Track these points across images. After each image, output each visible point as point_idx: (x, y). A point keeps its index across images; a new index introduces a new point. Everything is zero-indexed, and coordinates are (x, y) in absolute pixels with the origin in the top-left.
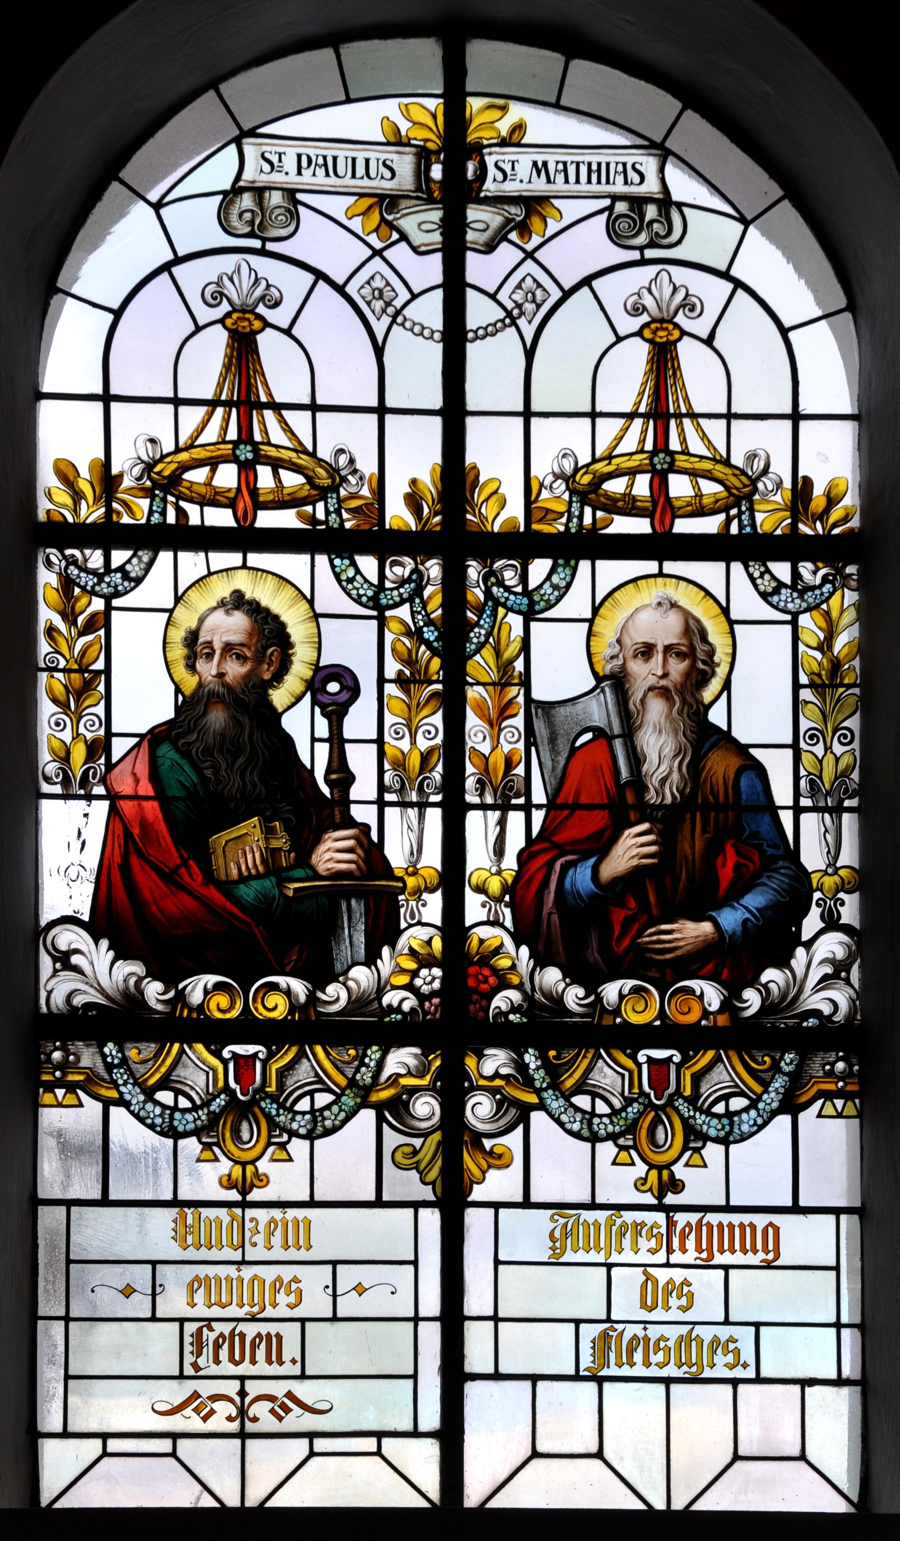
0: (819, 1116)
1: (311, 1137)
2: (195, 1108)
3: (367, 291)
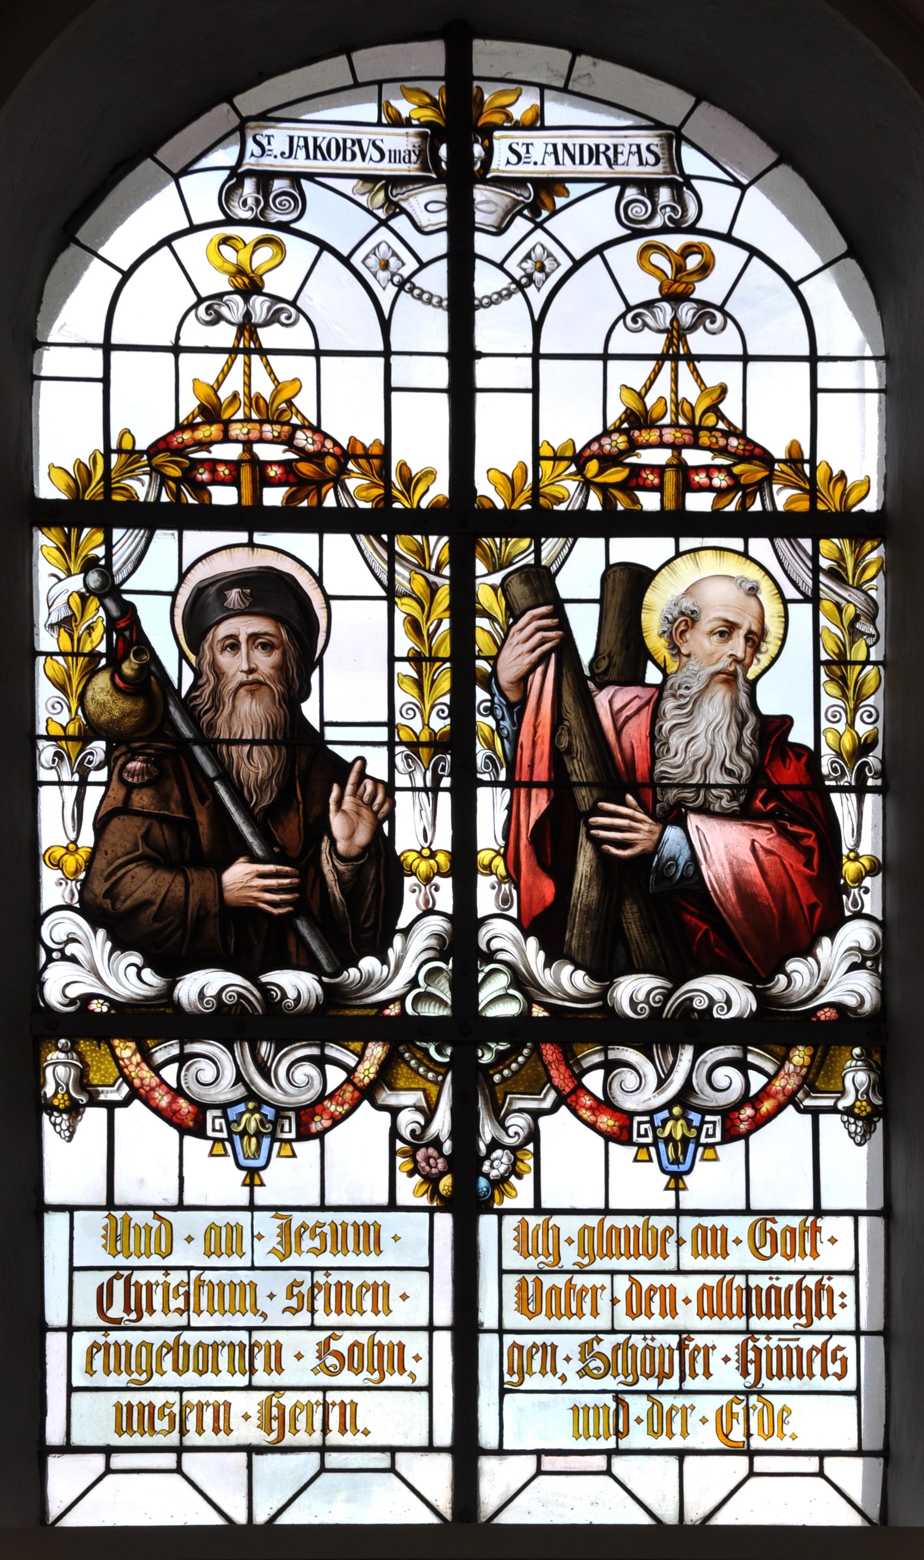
3: (372, 261)
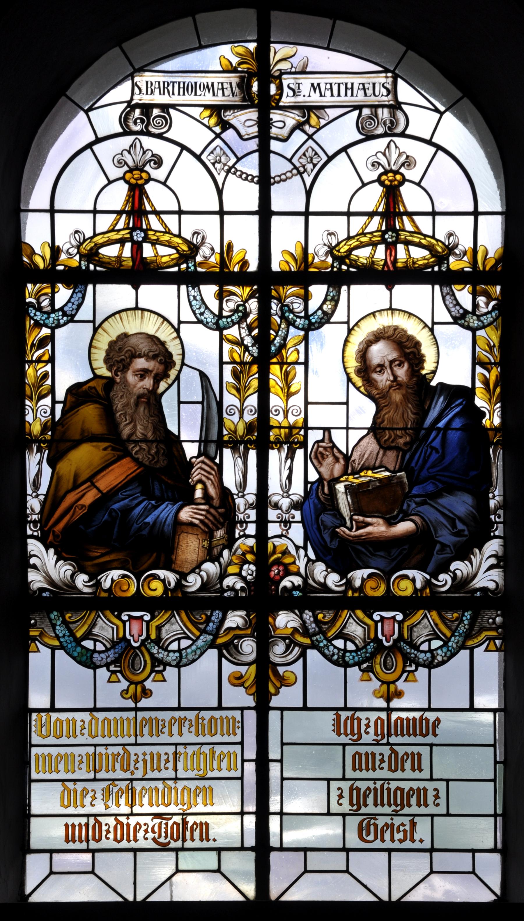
0: (486, 650)
1: (179, 666)
2: (107, 650)
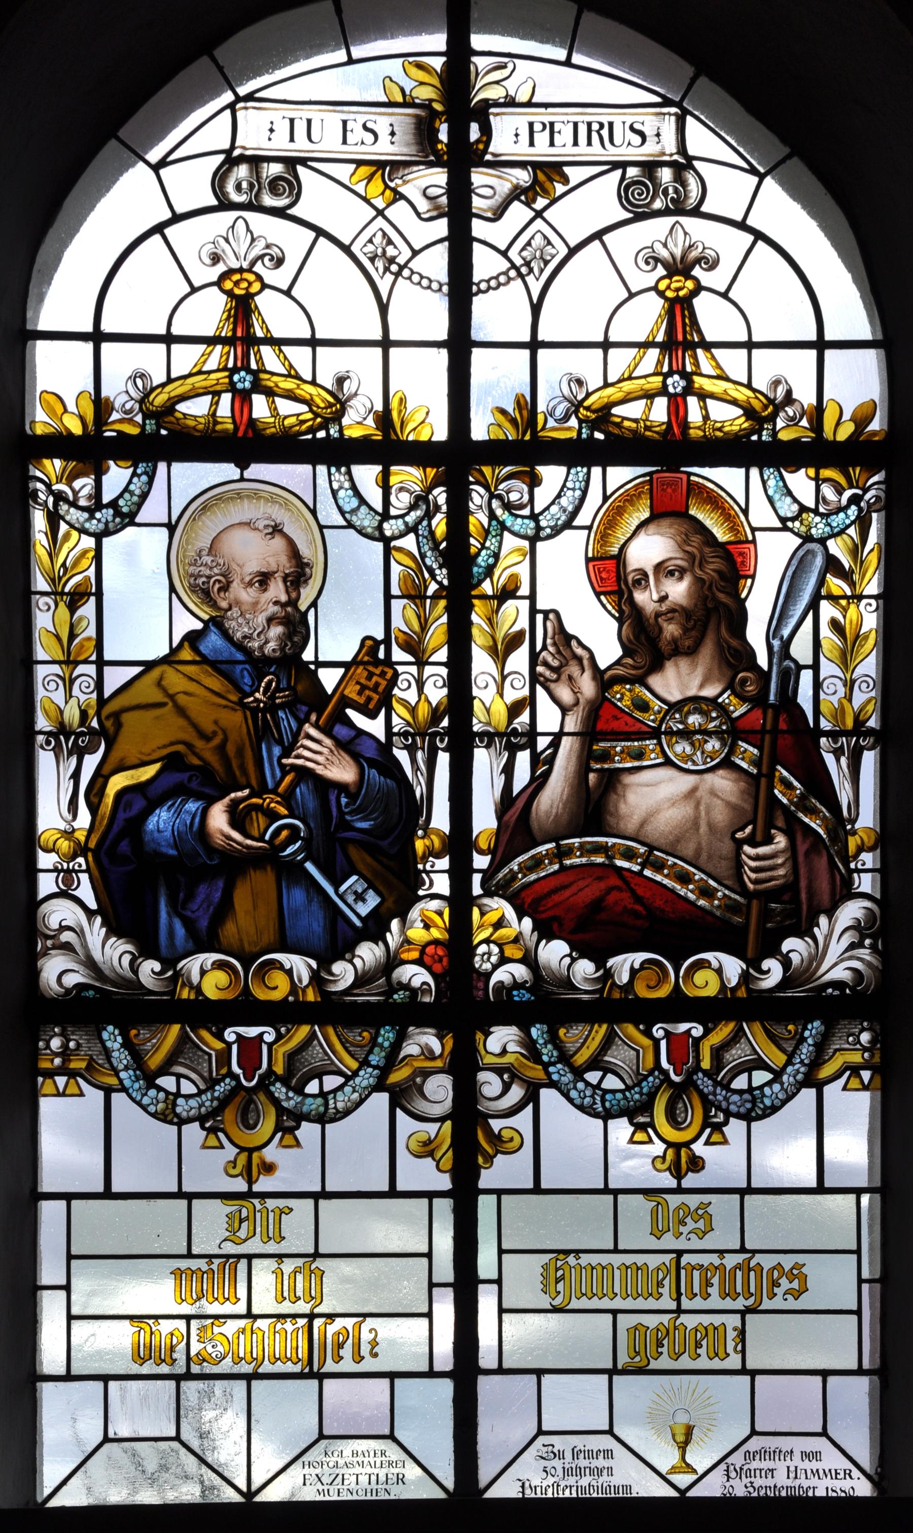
0: (845, 1088)
2: (200, 1093)
